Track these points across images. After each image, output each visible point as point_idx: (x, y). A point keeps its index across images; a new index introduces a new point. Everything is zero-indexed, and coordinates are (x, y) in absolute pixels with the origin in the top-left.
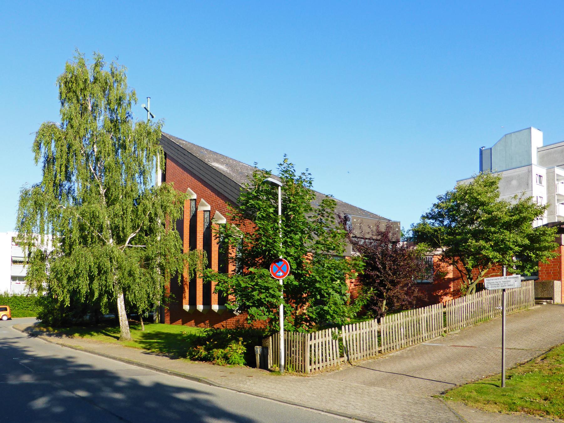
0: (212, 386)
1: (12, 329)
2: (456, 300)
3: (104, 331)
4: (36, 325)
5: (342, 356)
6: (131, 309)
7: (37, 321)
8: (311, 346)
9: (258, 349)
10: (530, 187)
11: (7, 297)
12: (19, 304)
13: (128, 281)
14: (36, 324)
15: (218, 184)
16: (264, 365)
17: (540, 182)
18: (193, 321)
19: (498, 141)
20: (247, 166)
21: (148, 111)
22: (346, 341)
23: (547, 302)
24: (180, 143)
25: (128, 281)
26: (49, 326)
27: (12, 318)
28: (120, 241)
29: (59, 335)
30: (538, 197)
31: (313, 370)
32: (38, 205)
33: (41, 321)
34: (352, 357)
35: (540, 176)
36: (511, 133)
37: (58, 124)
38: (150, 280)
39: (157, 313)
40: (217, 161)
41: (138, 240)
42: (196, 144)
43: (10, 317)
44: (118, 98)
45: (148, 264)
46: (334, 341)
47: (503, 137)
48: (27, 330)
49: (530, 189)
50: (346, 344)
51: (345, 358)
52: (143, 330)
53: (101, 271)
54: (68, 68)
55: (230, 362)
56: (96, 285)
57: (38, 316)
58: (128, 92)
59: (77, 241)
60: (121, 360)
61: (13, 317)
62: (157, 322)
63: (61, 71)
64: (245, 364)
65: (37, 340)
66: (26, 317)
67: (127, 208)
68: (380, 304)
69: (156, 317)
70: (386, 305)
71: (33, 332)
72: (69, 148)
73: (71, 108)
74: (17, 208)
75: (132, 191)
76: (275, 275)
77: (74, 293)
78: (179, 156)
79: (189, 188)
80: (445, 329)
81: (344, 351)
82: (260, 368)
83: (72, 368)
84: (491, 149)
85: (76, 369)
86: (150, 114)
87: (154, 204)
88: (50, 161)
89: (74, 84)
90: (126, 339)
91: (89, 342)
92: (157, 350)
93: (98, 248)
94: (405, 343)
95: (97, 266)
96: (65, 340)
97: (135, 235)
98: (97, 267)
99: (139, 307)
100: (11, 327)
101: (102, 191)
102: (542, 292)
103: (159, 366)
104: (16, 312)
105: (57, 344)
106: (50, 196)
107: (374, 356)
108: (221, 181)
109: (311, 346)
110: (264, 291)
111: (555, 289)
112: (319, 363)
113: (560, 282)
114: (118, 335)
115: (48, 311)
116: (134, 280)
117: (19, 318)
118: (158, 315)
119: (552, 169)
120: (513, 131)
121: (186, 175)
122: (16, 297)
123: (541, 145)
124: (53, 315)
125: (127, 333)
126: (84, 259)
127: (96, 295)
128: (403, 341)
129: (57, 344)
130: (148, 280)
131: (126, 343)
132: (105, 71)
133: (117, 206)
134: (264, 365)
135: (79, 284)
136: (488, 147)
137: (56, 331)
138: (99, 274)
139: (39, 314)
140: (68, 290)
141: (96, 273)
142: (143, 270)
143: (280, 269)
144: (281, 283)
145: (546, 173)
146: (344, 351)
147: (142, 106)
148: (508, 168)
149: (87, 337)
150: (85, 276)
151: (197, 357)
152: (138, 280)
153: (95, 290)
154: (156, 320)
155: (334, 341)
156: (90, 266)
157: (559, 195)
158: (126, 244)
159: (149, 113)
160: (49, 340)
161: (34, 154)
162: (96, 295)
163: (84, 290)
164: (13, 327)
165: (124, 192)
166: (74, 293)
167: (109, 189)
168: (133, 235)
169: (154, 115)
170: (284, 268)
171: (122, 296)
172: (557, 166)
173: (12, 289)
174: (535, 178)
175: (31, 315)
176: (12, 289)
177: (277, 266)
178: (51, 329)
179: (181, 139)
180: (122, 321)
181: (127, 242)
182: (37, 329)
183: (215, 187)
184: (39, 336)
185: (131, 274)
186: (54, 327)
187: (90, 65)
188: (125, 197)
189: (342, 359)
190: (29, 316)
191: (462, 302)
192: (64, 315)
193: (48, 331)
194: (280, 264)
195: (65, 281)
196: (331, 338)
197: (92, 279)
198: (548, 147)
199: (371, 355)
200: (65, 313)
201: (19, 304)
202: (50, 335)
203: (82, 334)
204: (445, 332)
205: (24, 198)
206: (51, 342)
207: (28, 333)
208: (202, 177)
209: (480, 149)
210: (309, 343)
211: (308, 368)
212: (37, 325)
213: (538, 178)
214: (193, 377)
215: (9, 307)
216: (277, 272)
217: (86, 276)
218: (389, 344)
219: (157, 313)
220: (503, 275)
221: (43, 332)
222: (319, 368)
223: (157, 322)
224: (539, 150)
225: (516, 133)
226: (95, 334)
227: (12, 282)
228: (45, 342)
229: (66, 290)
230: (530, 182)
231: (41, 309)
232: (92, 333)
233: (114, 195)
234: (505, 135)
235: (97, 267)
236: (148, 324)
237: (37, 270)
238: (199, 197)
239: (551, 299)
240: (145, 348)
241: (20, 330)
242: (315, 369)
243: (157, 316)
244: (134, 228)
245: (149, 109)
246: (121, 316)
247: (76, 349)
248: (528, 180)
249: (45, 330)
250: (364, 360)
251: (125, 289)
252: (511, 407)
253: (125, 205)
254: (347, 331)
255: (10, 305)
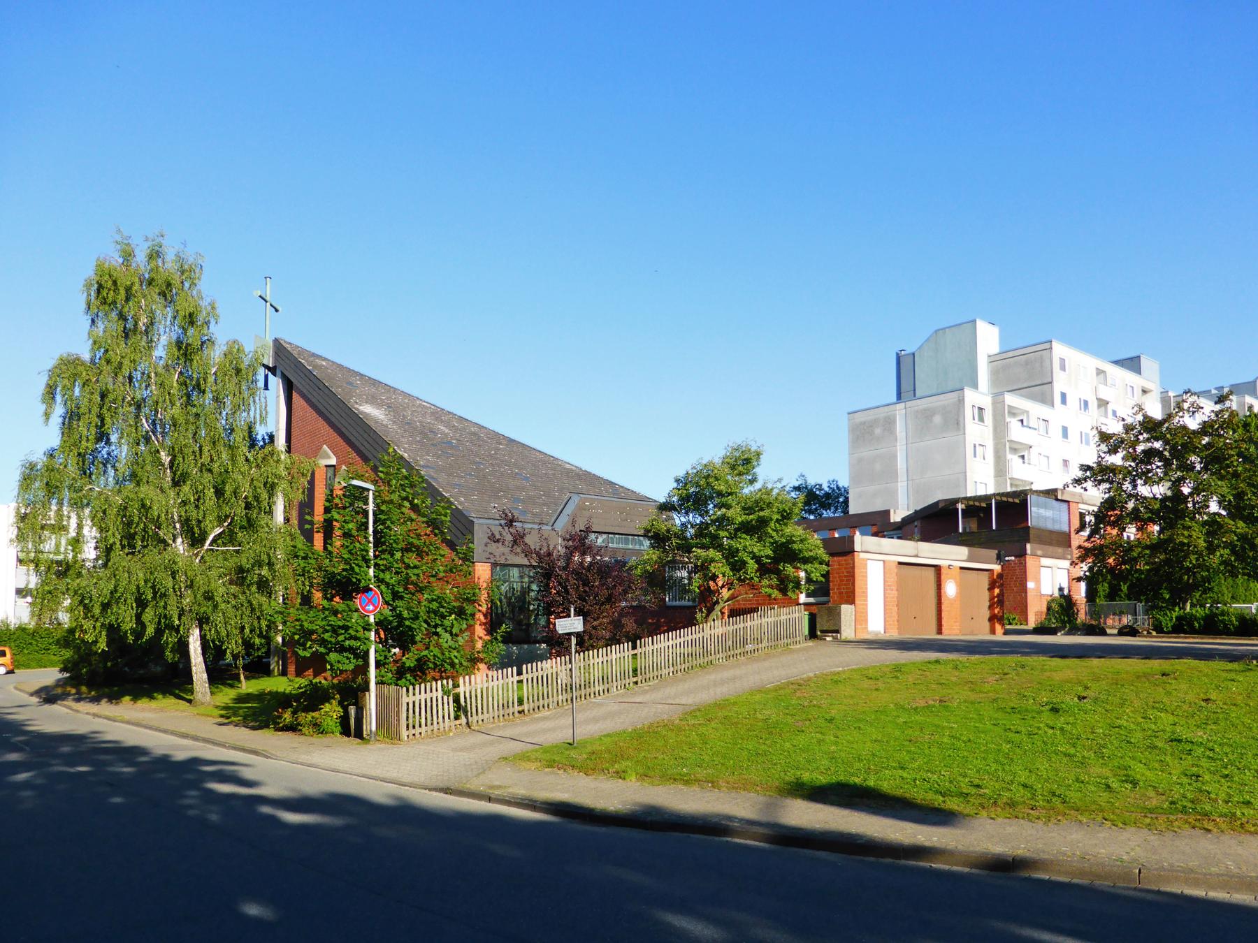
0: (269, 760)
1: (13, 690)
2: (655, 637)
3: (177, 692)
4: (59, 683)
5: (457, 718)
6: (213, 652)
7: (60, 676)
8: (408, 704)
9: (352, 710)
10: (961, 428)
11: (8, 629)
12: (31, 644)
13: (205, 608)
14: (59, 680)
15: (365, 444)
16: (359, 735)
17: (981, 419)
18: (311, 670)
19: (926, 341)
20: (429, 405)
21: (266, 302)
22: (465, 698)
23: (832, 636)
24: (315, 366)
25: (206, 608)
26: (82, 685)
27: (15, 671)
28: (196, 540)
29: (96, 700)
30: (977, 446)
31: (411, 737)
32: (51, 489)
33: (68, 675)
34: (473, 720)
35: (980, 409)
36: (944, 329)
37: (86, 356)
38: (245, 605)
39: (276, 659)
40: (373, 400)
41: (229, 537)
42: (345, 364)
43: (11, 667)
44: (187, 314)
45: (244, 579)
46: (445, 698)
47: (930, 336)
48: (37, 693)
49: (962, 432)
50: (465, 702)
51: (463, 720)
52: (244, 687)
53: (157, 592)
54: (100, 268)
55: (322, 730)
56: (148, 615)
57: (62, 666)
58: (204, 304)
59: (118, 545)
60: (173, 733)
61: (18, 668)
62: (276, 674)
63: (89, 272)
64: (341, 733)
65: (57, 708)
66: (45, 667)
67: (204, 489)
68: (566, 644)
69: (275, 665)
70: (576, 645)
71: (49, 696)
72: (103, 396)
73: (108, 326)
74: (15, 492)
75: (212, 460)
76: (364, 609)
77: (113, 631)
78: (311, 390)
79: (325, 446)
80: (635, 679)
81: (460, 709)
82: (355, 737)
83: (89, 745)
84: (914, 354)
85: (96, 745)
86: (271, 305)
87: (252, 480)
88: (72, 417)
89: (112, 292)
90: (203, 704)
91: (143, 710)
92: (239, 718)
93: (153, 556)
94: (564, 700)
95: (150, 584)
96: (104, 708)
97: (222, 530)
98: (151, 587)
99: (226, 649)
100: (11, 687)
101: (165, 458)
102: (828, 621)
103: (238, 743)
104: (24, 659)
105: (87, 714)
106: (73, 469)
107: (511, 717)
108: (369, 439)
109: (408, 704)
110: (343, 632)
111: (842, 616)
112: (420, 726)
113: (853, 606)
114: (191, 698)
115: (81, 657)
116: (216, 606)
117: (28, 670)
118: (278, 662)
119: (1001, 397)
120: (948, 325)
121: (321, 423)
122: (25, 629)
123: (995, 349)
124: (90, 664)
125: (204, 694)
126: (126, 575)
127: (150, 630)
128: (560, 697)
129: (87, 714)
130: (242, 605)
131: (202, 710)
132: (169, 264)
133: (186, 489)
134: (359, 735)
135: (118, 614)
136: (909, 351)
137: (93, 693)
138: (154, 598)
139: (65, 662)
140: (103, 625)
141: (150, 596)
142: (233, 589)
143: (370, 601)
144: (372, 620)
145: (992, 404)
146: (460, 709)
147: (254, 294)
148: (940, 391)
149: (144, 703)
150: (129, 601)
151: (281, 725)
152: (222, 606)
153: (148, 624)
154: (274, 670)
155: (445, 698)
156: (138, 587)
157: (1011, 441)
158: (207, 546)
159: (268, 304)
160: (75, 708)
161: (44, 406)
162: (150, 630)
163: (128, 625)
164: (16, 688)
165: (199, 465)
166: (113, 631)
167: (174, 457)
168: (218, 531)
169: (278, 307)
170: (375, 601)
171: (197, 632)
172: (1008, 391)
173: (17, 614)
174: (968, 412)
175: (52, 664)
176: (17, 614)
177: (367, 598)
178: (84, 689)
179: (319, 357)
180: (196, 673)
181: (208, 542)
182: (59, 691)
183: (362, 448)
184: (59, 702)
185: (209, 597)
186: (91, 685)
187: (141, 257)
188: (201, 471)
189: (458, 722)
190: (50, 666)
191: (674, 637)
192: (109, 664)
193: (78, 693)
194: (370, 594)
195: (97, 610)
196: (440, 693)
197: (141, 604)
198: (1011, 354)
199: (506, 717)
200: (111, 661)
201: (31, 644)
202: (78, 700)
203: (136, 697)
204: (636, 683)
205: (29, 476)
206: (77, 711)
207: (41, 698)
208: (343, 430)
209: (897, 354)
210: (404, 700)
211: (404, 733)
212: (61, 683)
213: (976, 411)
214: (478, 794)
215: (10, 648)
216: (366, 605)
217: (131, 601)
218: (536, 701)
219: (276, 659)
220: (569, 616)
221: (69, 694)
222: (420, 733)
223: (276, 674)
224: (992, 359)
225: (953, 328)
226: (160, 696)
227: (17, 599)
228: (68, 711)
229: (98, 624)
230: (961, 419)
231: (67, 654)
232: (155, 694)
233: (181, 469)
234: (936, 331)
235: (151, 587)
236: (263, 677)
237: (50, 592)
238: (340, 462)
239: (838, 631)
240: (222, 716)
241: (27, 693)
242: (414, 735)
243: (275, 664)
244: (220, 520)
245: (268, 298)
246: (195, 666)
247: (115, 721)
248: (958, 416)
249: (73, 691)
250: (493, 723)
251: (202, 621)
252: (281, 730)
253: (201, 484)
254: (467, 684)
255: (13, 644)
